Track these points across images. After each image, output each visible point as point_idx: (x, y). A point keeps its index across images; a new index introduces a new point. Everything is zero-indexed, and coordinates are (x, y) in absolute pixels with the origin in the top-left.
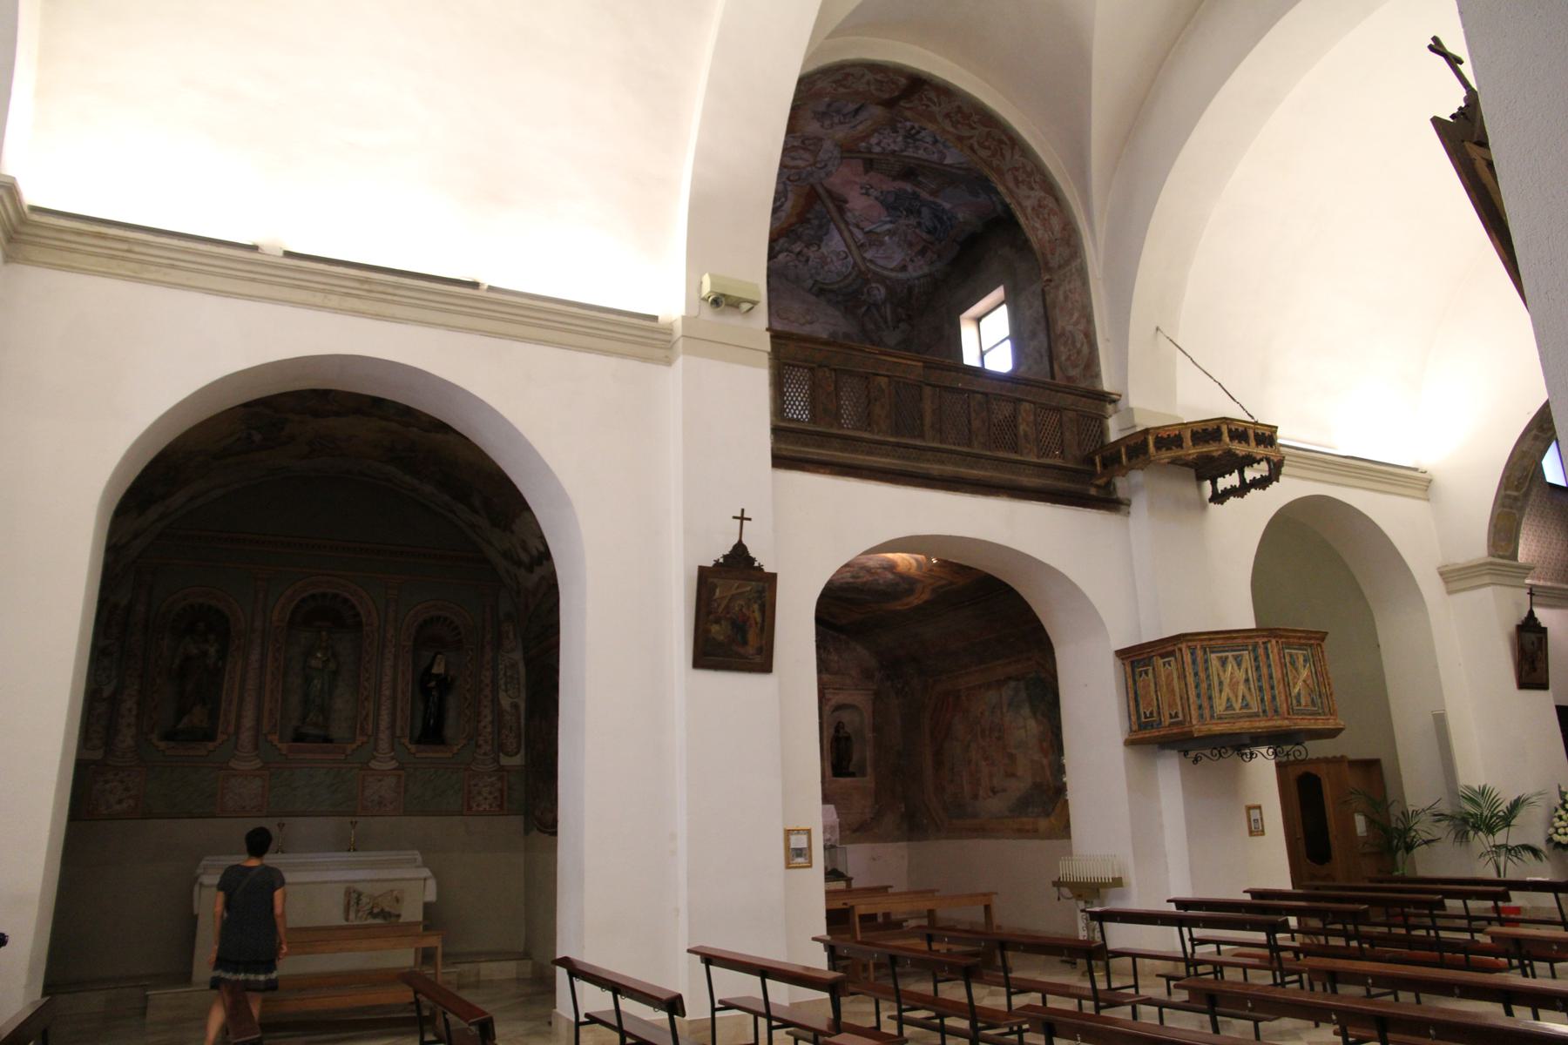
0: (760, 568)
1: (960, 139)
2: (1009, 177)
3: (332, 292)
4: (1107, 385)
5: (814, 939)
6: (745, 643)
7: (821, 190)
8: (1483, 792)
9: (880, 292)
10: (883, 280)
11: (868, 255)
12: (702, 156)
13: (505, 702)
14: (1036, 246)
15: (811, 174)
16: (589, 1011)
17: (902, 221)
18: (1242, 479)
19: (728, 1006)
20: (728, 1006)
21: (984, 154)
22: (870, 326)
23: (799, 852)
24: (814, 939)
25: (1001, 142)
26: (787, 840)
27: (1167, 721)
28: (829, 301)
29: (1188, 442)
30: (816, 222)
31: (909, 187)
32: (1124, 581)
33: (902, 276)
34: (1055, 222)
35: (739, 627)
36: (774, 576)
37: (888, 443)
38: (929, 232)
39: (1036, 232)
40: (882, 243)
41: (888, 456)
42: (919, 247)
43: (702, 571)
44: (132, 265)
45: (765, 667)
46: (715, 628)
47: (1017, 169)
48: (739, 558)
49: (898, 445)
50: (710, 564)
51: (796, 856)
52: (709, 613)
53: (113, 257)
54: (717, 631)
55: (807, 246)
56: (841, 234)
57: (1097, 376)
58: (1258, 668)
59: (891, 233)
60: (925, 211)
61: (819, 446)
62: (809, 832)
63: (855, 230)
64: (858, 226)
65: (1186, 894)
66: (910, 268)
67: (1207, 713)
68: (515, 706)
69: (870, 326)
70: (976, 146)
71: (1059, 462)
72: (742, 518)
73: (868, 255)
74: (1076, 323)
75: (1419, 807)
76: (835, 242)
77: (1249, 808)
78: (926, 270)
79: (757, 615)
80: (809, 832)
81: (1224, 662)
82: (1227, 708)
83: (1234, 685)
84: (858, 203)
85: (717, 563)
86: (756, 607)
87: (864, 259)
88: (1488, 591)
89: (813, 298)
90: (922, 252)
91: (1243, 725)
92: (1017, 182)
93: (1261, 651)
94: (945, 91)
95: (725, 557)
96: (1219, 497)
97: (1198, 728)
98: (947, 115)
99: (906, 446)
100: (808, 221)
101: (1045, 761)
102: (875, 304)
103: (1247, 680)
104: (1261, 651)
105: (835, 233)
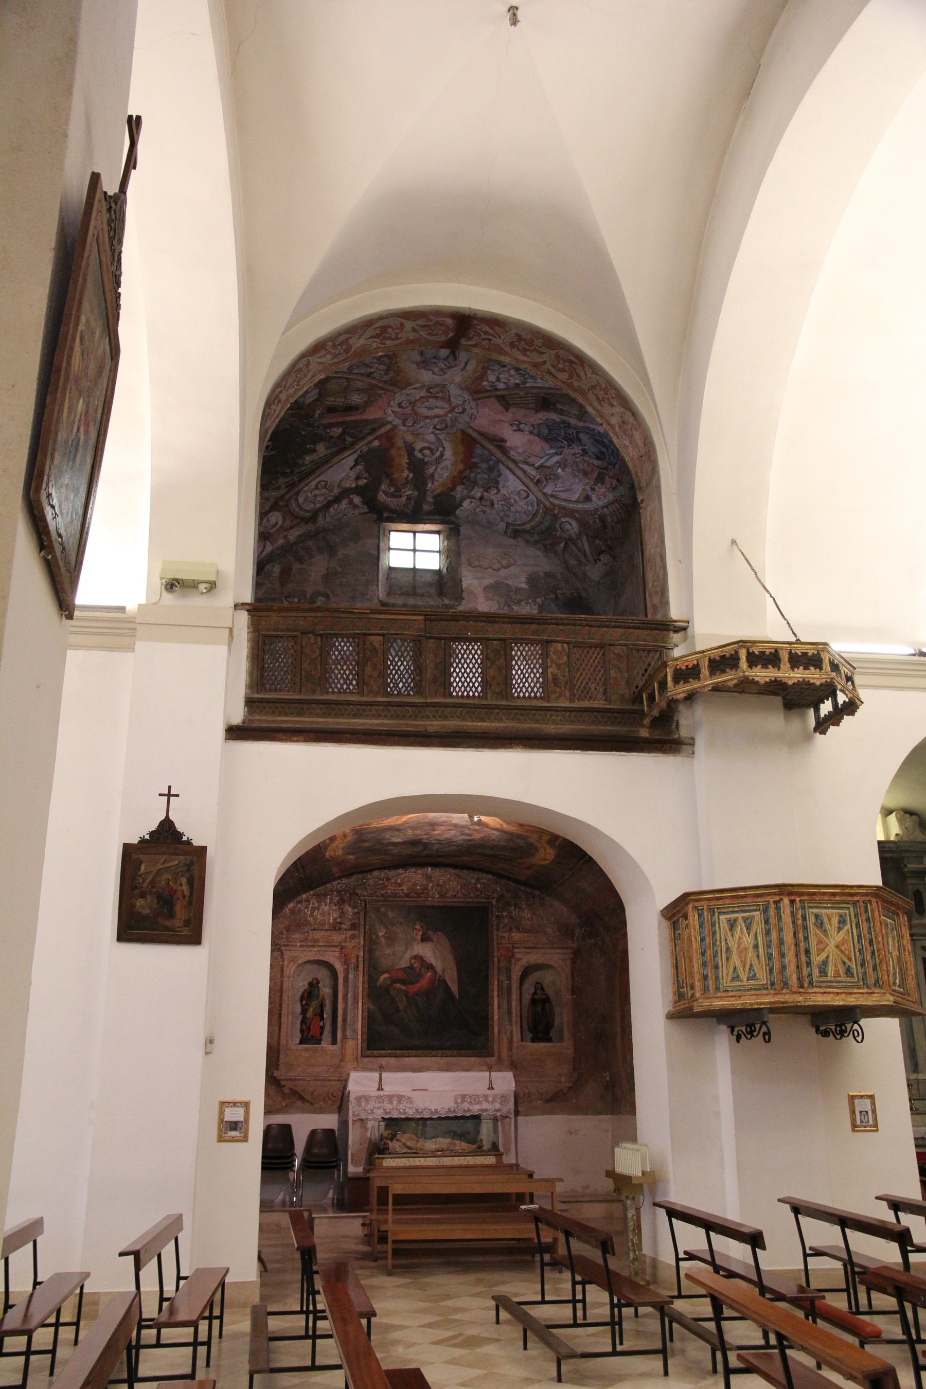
0: (189, 842)
1: (536, 366)
2: (591, 396)
4: (675, 612)
6: (171, 915)
7: (474, 435)
9: (572, 527)
10: (571, 513)
11: (548, 490)
15: (455, 420)
16: (688, 1249)
17: (566, 451)
19: (818, 1253)
20: (818, 1253)
21: (564, 376)
22: (573, 562)
23: (234, 1126)
25: (571, 362)
26: (221, 1113)
28: (527, 542)
29: (705, 671)
30: (484, 466)
31: (555, 417)
33: (587, 506)
34: (637, 436)
35: (166, 901)
36: (203, 849)
37: (379, 704)
38: (598, 458)
40: (557, 477)
41: (379, 716)
42: (594, 476)
43: (127, 848)
45: (195, 938)
46: (140, 903)
47: (594, 387)
48: (167, 834)
50: (135, 841)
51: (232, 1129)
52: (134, 888)
54: (142, 905)
55: (487, 490)
56: (514, 473)
58: (768, 932)
59: (563, 464)
60: (582, 436)
61: (299, 714)
62: (246, 1105)
63: (526, 467)
64: (527, 463)
66: (594, 497)
67: (710, 983)
69: (573, 562)
70: (552, 370)
71: (597, 704)
73: (548, 490)
76: (511, 484)
77: (852, 1098)
78: (610, 496)
79: (185, 888)
80: (246, 1105)
81: (732, 924)
82: (733, 980)
84: (516, 441)
85: (143, 841)
86: (184, 880)
87: (545, 495)
89: (511, 541)
90: (600, 479)
93: (772, 911)
94: (496, 323)
95: (152, 834)
96: (822, 726)
98: (512, 345)
100: (475, 465)
102: (570, 539)
103: (756, 946)
104: (772, 911)
105: (511, 477)
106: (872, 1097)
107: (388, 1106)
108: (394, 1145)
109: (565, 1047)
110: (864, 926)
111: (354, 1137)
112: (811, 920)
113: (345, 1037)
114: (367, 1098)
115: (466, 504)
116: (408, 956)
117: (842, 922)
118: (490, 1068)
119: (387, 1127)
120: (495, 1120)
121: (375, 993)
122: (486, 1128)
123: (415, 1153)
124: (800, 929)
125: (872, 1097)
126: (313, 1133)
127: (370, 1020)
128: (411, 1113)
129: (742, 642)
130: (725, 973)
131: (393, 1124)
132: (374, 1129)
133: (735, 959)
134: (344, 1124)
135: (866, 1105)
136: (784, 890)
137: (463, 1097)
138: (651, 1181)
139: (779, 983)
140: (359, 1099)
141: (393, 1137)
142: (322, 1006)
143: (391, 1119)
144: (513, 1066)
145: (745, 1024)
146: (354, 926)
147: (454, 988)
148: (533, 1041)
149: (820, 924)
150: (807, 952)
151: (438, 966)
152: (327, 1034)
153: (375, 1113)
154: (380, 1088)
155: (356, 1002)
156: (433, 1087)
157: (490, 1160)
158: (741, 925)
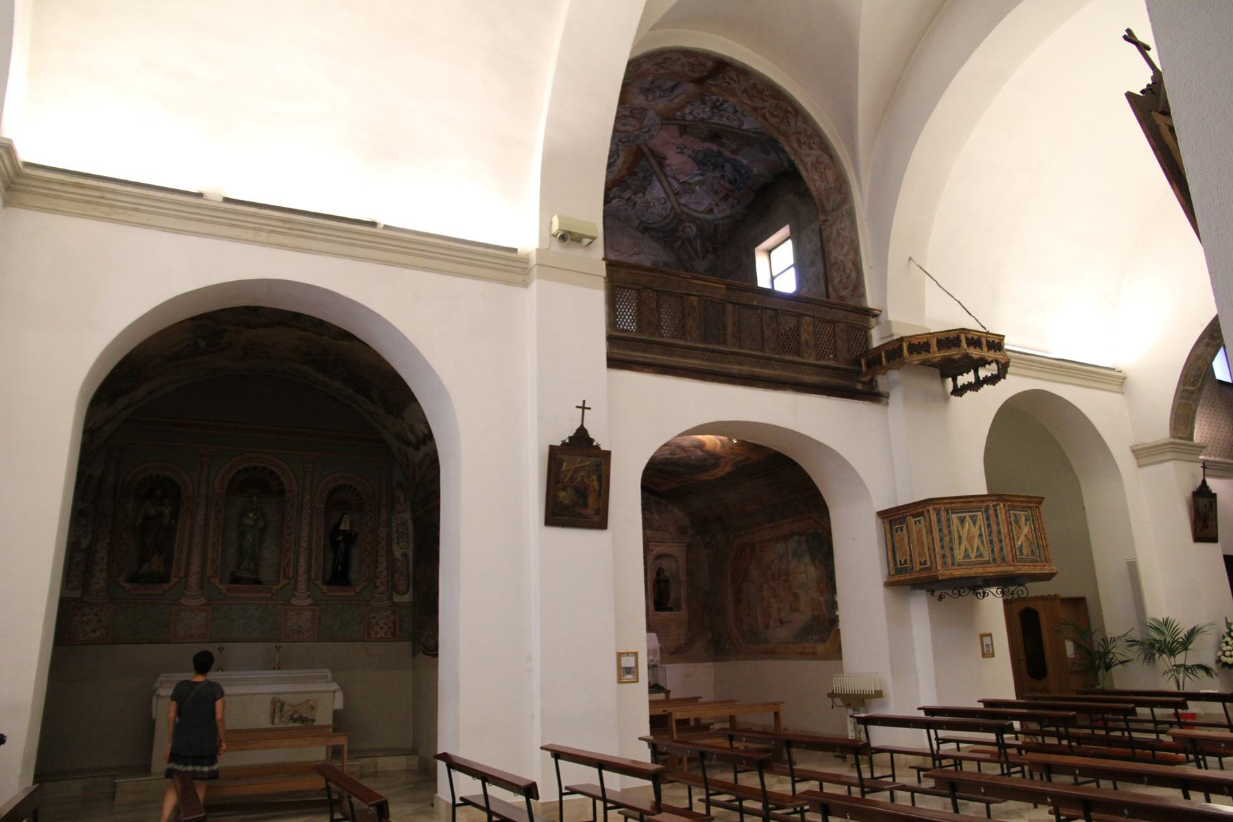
0: (598, 447)
1: (755, 109)
2: (793, 139)
3: (261, 230)
4: (871, 303)
5: (640, 739)
6: (586, 506)
7: (645, 150)
8: (1166, 623)
9: (692, 230)
10: (694, 220)
11: (683, 201)
12: (552, 123)
13: (397, 552)
14: (814, 194)
15: (637, 137)
17: (709, 174)
18: (977, 377)
21: (774, 121)
22: (684, 257)
23: (628, 670)
24: (640, 739)
25: (787, 111)
26: (619, 661)
27: (917, 567)
28: (652, 237)
29: (934, 347)
30: (641, 175)
31: (715, 147)
32: (884, 457)
33: (709, 217)
34: (830, 174)
35: (581, 494)
36: (608, 453)
37: (698, 349)
38: (730, 183)
39: (815, 182)
40: (694, 192)
41: (698, 358)
42: (723, 195)
43: (552, 449)
44: (104, 209)
45: (602, 524)
46: (562, 494)
47: (800, 133)
48: (581, 439)
49: (706, 350)
50: (558, 443)
51: (626, 673)
52: (558, 482)
53: (89, 202)
54: (564, 496)
55: (635, 194)
56: (661, 184)
57: (863, 295)
58: (989, 525)
59: (700, 183)
60: (727, 166)
61: (644, 351)
62: (636, 654)
63: (672, 181)
64: (674, 178)
65: (933, 703)
66: (716, 211)
67: (949, 561)
68: (405, 555)
69: (684, 257)
70: (767, 115)
71: (832, 364)
72: (583, 408)
73: (683, 201)
74: (846, 254)
75: (1116, 635)
76: (657, 190)
77: (982, 636)
78: (728, 212)
79: (595, 484)
80: (636, 654)
81: (962, 521)
82: (965, 557)
83: (970, 539)
84: (675, 160)
85: (564, 443)
86: (594, 477)
87: (679, 204)
88: (1170, 465)
89: (639, 235)
90: (725, 199)
91: (978, 571)
92: (800, 143)
93: (991, 512)
94: (743, 72)
95: (570, 438)
96: (959, 391)
97: (942, 572)
98: (745, 91)
99: (713, 351)
100: (635, 174)
101: (822, 599)
102: (688, 239)
103: (981, 535)
104: (991, 512)
105: (657, 183)
109: (682, 615)
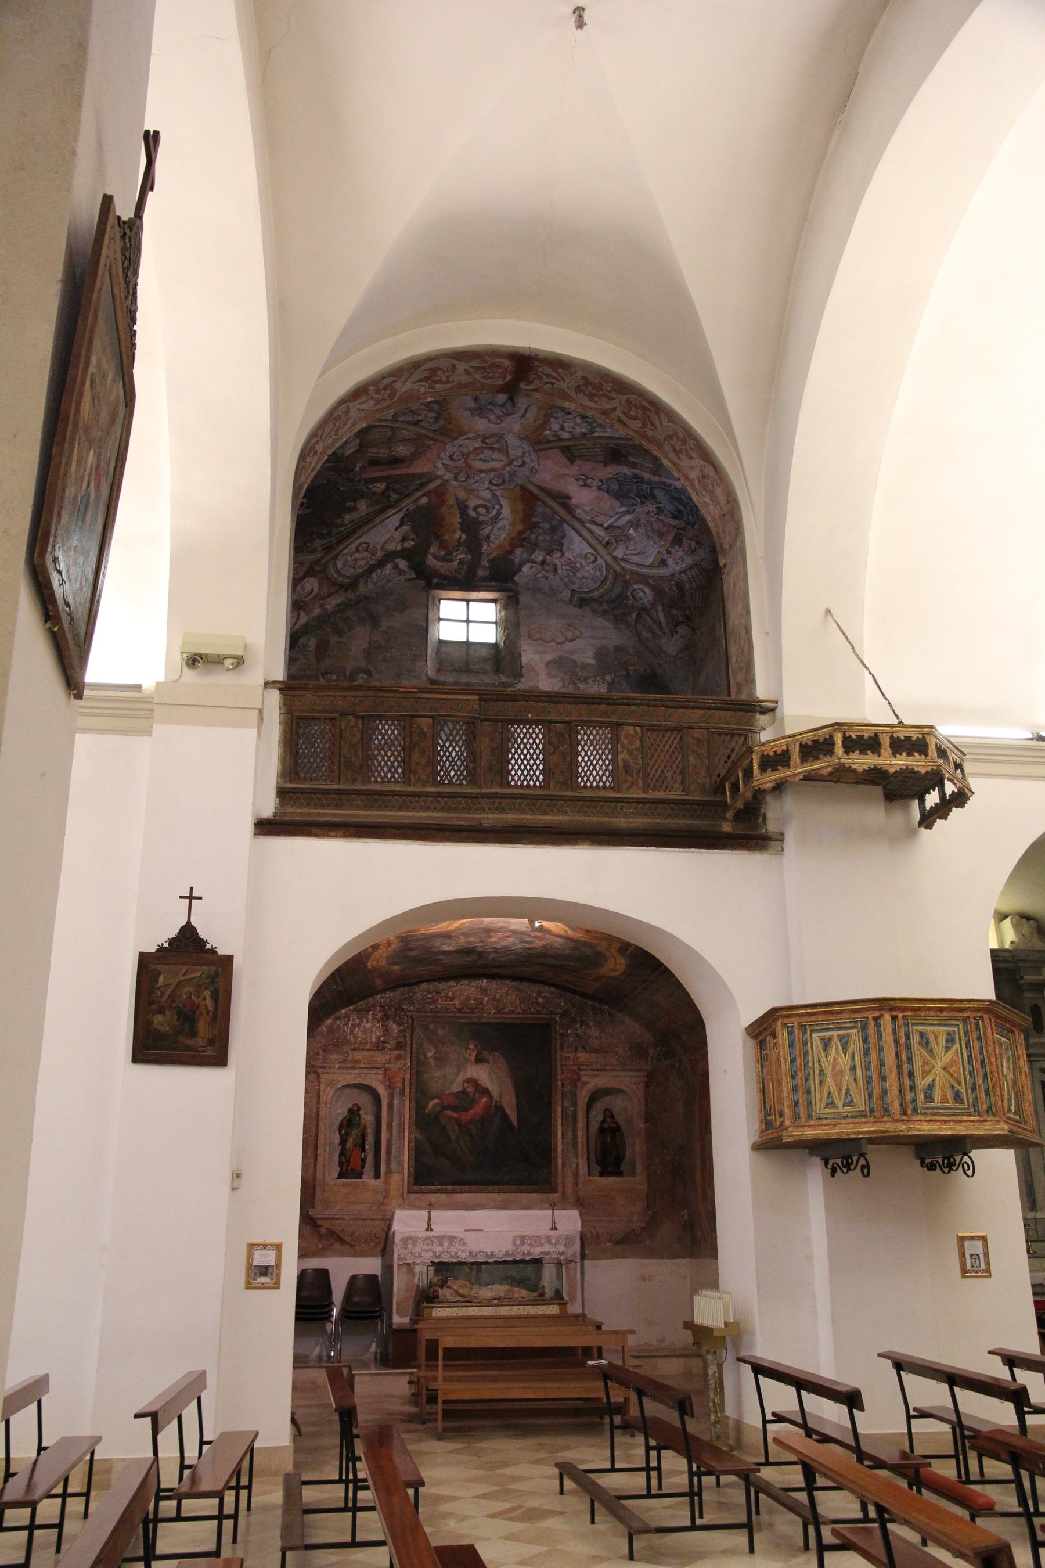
0: (213, 951)
1: (605, 413)
2: (667, 447)
4: (762, 691)
6: (193, 1033)
7: (535, 491)
9: (646, 595)
10: (644, 579)
11: (619, 553)
15: (513, 474)
17: (639, 509)
21: (636, 425)
22: (646, 635)
23: (264, 1271)
25: (644, 408)
26: (250, 1257)
28: (595, 612)
29: (795, 758)
30: (547, 526)
31: (626, 470)
33: (663, 571)
34: (719, 492)
35: (188, 1017)
36: (230, 959)
37: (428, 795)
38: (675, 517)
40: (629, 538)
41: (427, 809)
42: (671, 537)
43: (143, 957)
45: (220, 1059)
46: (158, 1019)
47: (670, 437)
48: (188, 942)
50: (152, 949)
51: (262, 1275)
52: (151, 1003)
54: (161, 1022)
55: (549, 553)
56: (580, 534)
58: (867, 1052)
59: (635, 524)
60: (656, 492)
61: (337, 806)
62: (278, 1247)
63: (593, 527)
64: (595, 523)
66: (670, 561)
67: (802, 1109)
69: (646, 635)
70: (623, 418)
71: (673, 795)
73: (619, 553)
76: (577, 546)
77: (961, 1240)
78: (689, 560)
79: (209, 1002)
80: (278, 1247)
81: (826, 1044)
82: (827, 1106)
84: (582, 497)
85: (161, 949)
86: (207, 994)
87: (615, 558)
89: (576, 611)
90: (677, 541)
93: (871, 1029)
94: (559, 364)
95: (171, 941)
96: (927, 819)
98: (578, 389)
100: (536, 525)
102: (644, 609)
103: (853, 1068)
104: (871, 1029)
105: (577, 538)
106: (984, 1239)
107: (438, 1249)
108: (445, 1293)
109: (638, 1182)
110: (975, 1046)
111: (399, 1283)
112: (915, 1039)
113: (389, 1171)
114: (414, 1240)
115: (525, 569)
116: (460, 1079)
117: (950, 1040)
118: (553, 1206)
119: (437, 1272)
120: (559, 1264)
121: (424, 1121)
122: (548, 1274)
123: (468, 1302)
124: (903, 1048)
125: (984, 1239)
126: (354, 1278)
127: (417, 1151)
128: (463, 1257)
129: (838, 725)
130: (819, 1098)
131: (444, 1269)
132: (423, 1275)
133: (830, 1083)
134: (388, 1268)
135: (977, 1247)
136: (884, 1004)
137: (523, 1238)
138: (735, 1333)
139: (879, 1110)
140: (405, 1240)
141: (443, 1284)
142: (363, 1136)
143: (441, 1263)
144: (579, 1203)
145: (841, 1156)
146: (399, 1046)
147: (513, 1115)
148: (601, 1175)
149: (925, 1043)
150: (911, 1074)
151: (495, 1090)
152: (369, 1167)
153: (423, 1256)
154: (429, 1229)
155: (401, 1131)
156: (488, 1227)
157: (553, 1309)
158: (836, 1044)
